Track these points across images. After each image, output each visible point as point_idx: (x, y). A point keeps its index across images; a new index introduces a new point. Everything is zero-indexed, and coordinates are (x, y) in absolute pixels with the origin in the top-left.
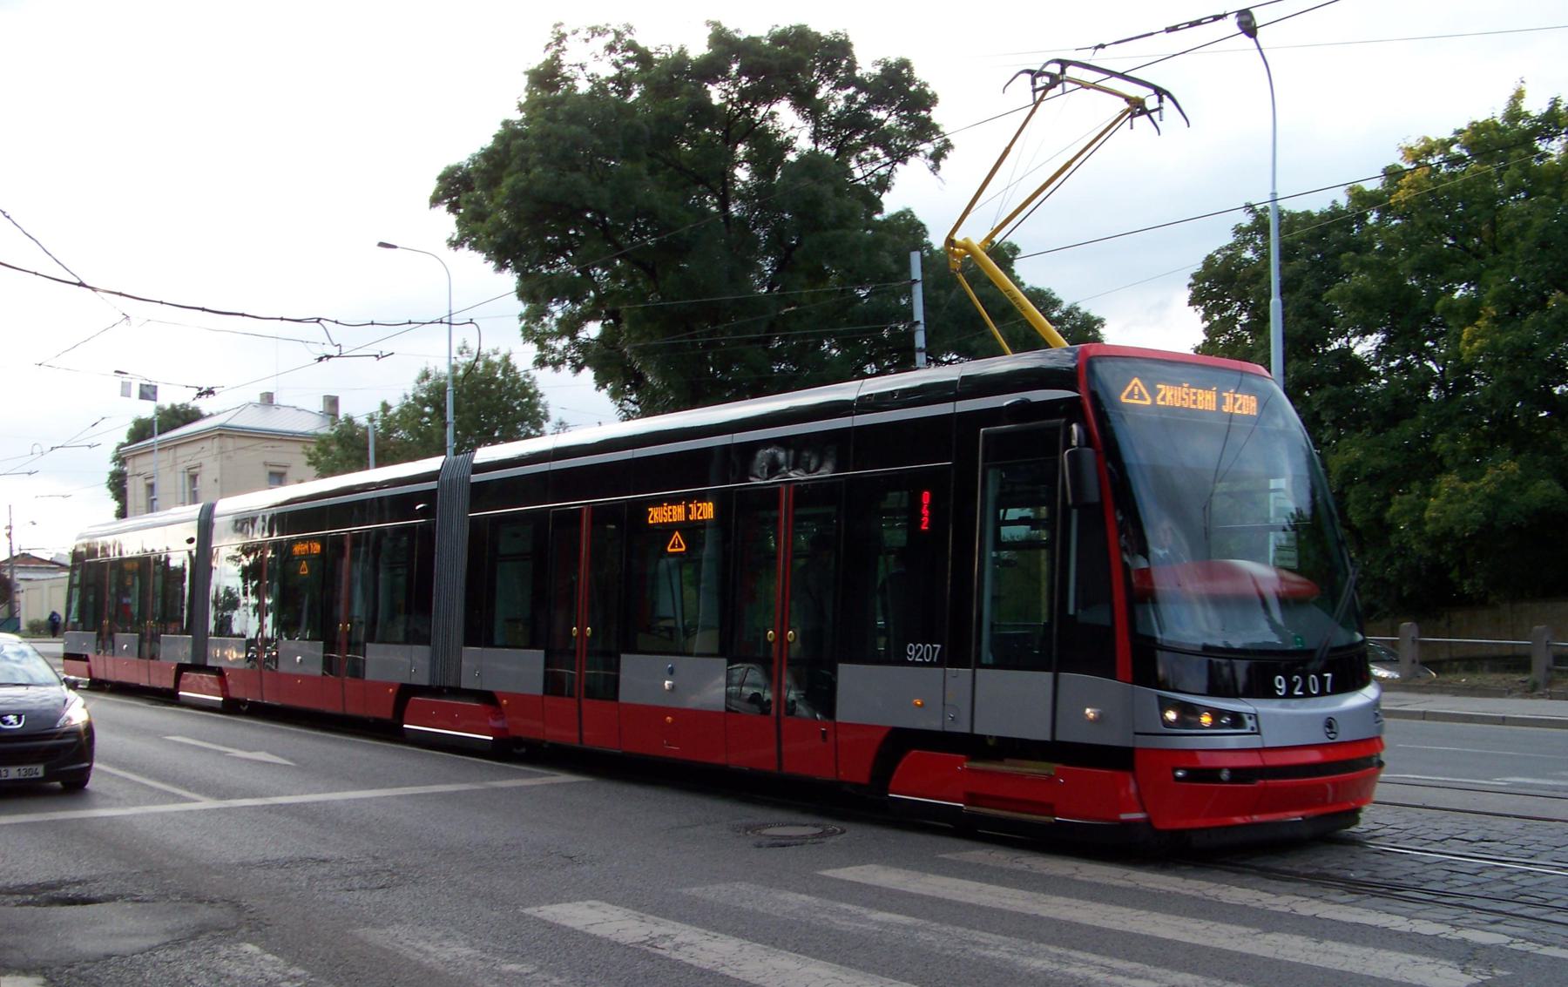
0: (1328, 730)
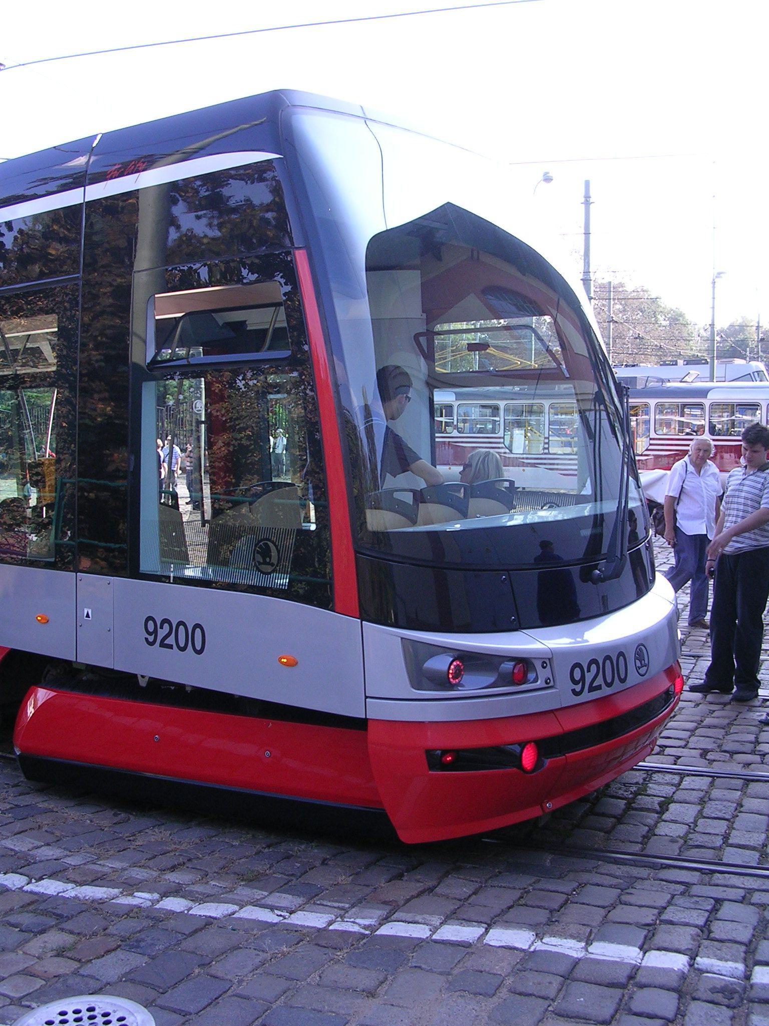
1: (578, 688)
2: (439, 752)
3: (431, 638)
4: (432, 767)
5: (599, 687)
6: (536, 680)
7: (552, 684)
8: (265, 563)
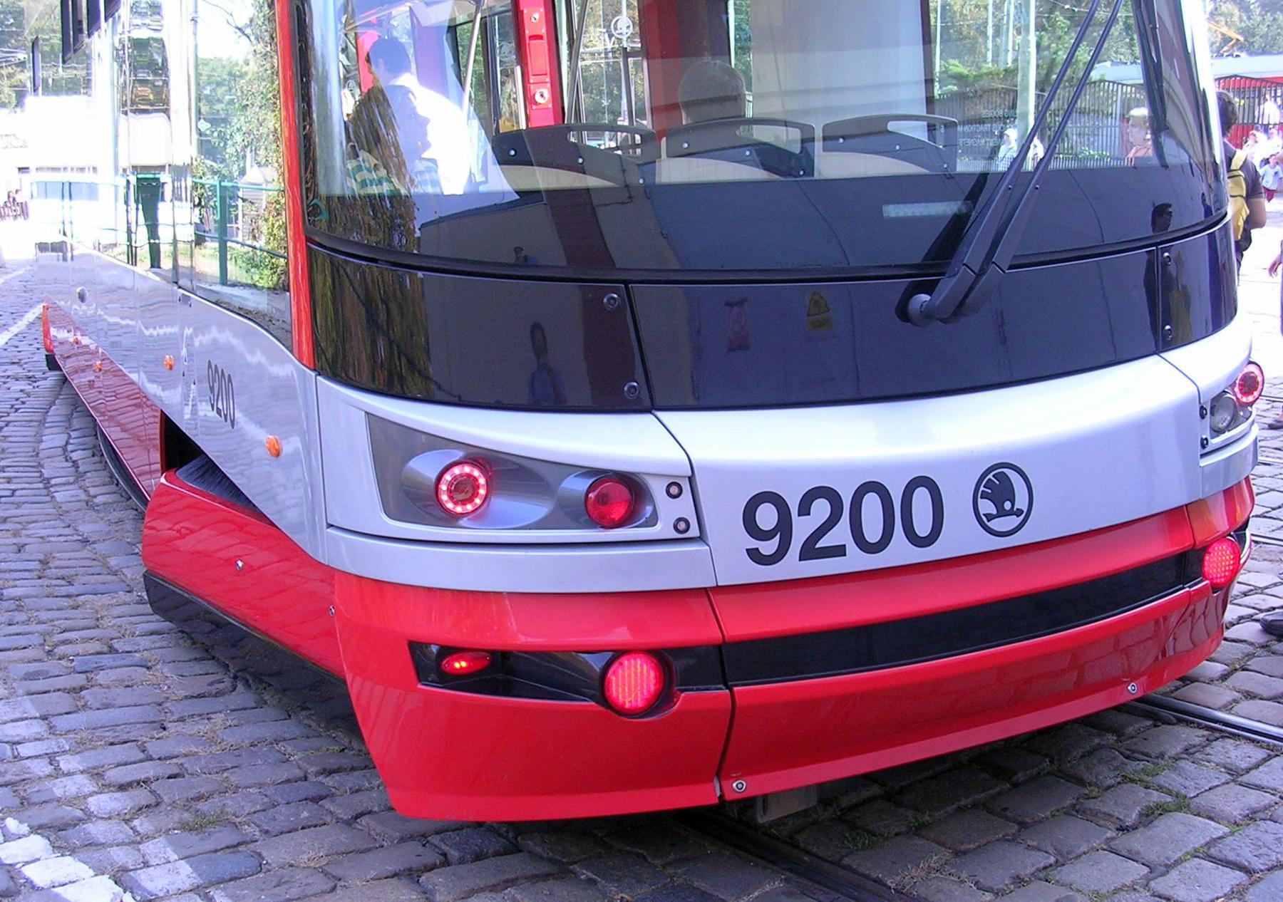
0: (987, 507)
1: (768, 547)
2: (434, 649)
3: (403, 413)
4: (421, 677)
5: (839, 551)
6: (652, 521)
7: (694, 531)
8: (1002, 513)
